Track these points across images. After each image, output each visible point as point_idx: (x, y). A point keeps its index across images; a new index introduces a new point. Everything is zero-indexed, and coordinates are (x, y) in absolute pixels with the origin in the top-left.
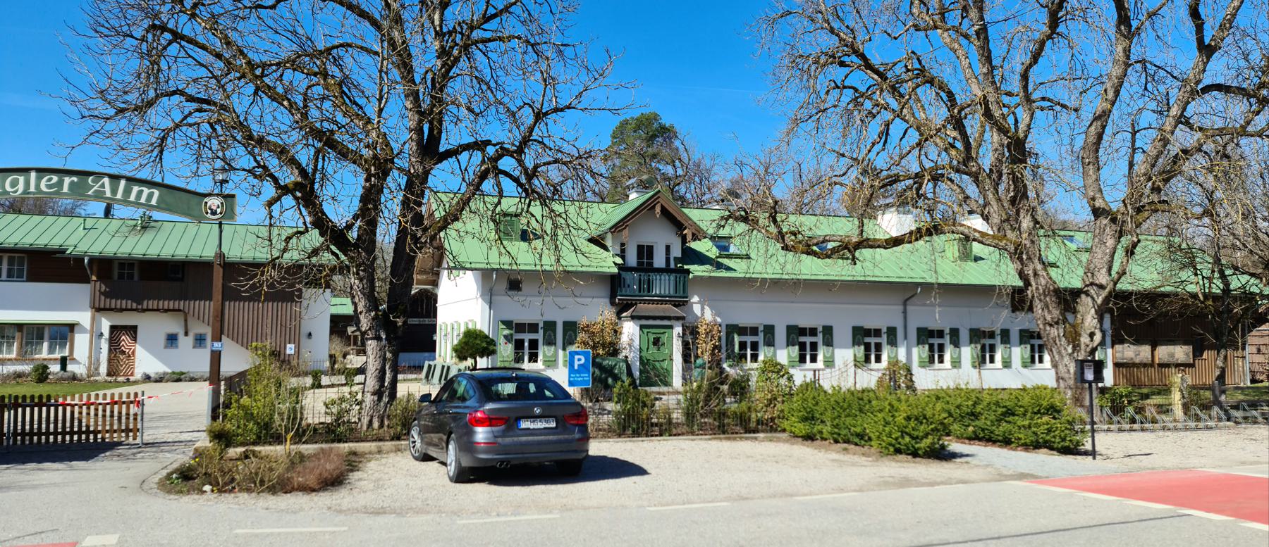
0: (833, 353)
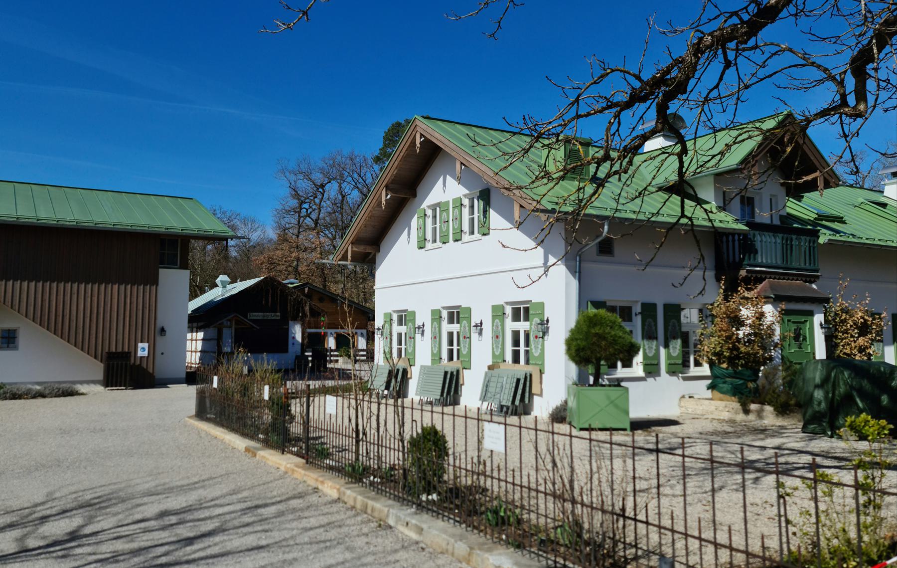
0: (883, 351)
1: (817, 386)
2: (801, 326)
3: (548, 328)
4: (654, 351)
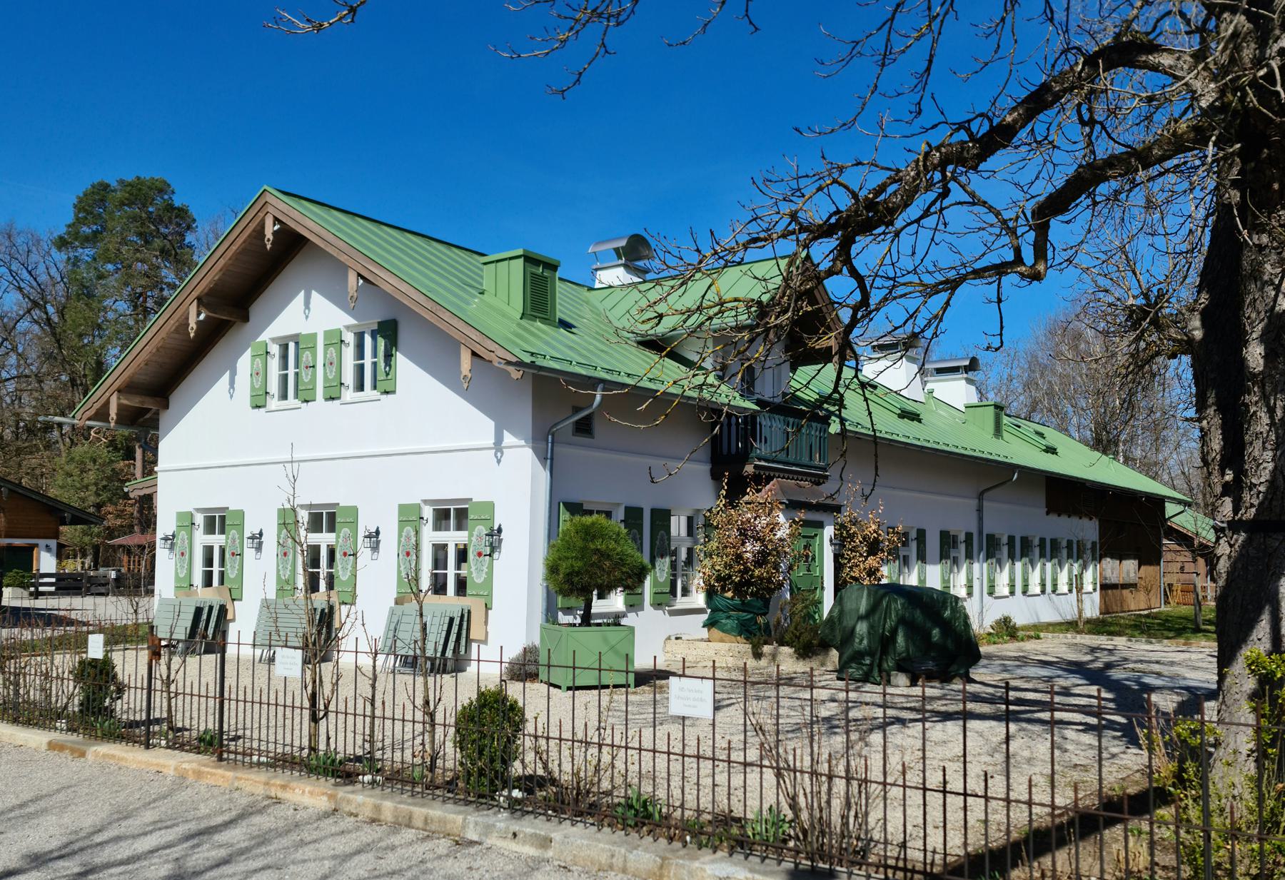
1: (861, 618)
2: (811, 541)
3: (500, 541)
4: (484, 576)
